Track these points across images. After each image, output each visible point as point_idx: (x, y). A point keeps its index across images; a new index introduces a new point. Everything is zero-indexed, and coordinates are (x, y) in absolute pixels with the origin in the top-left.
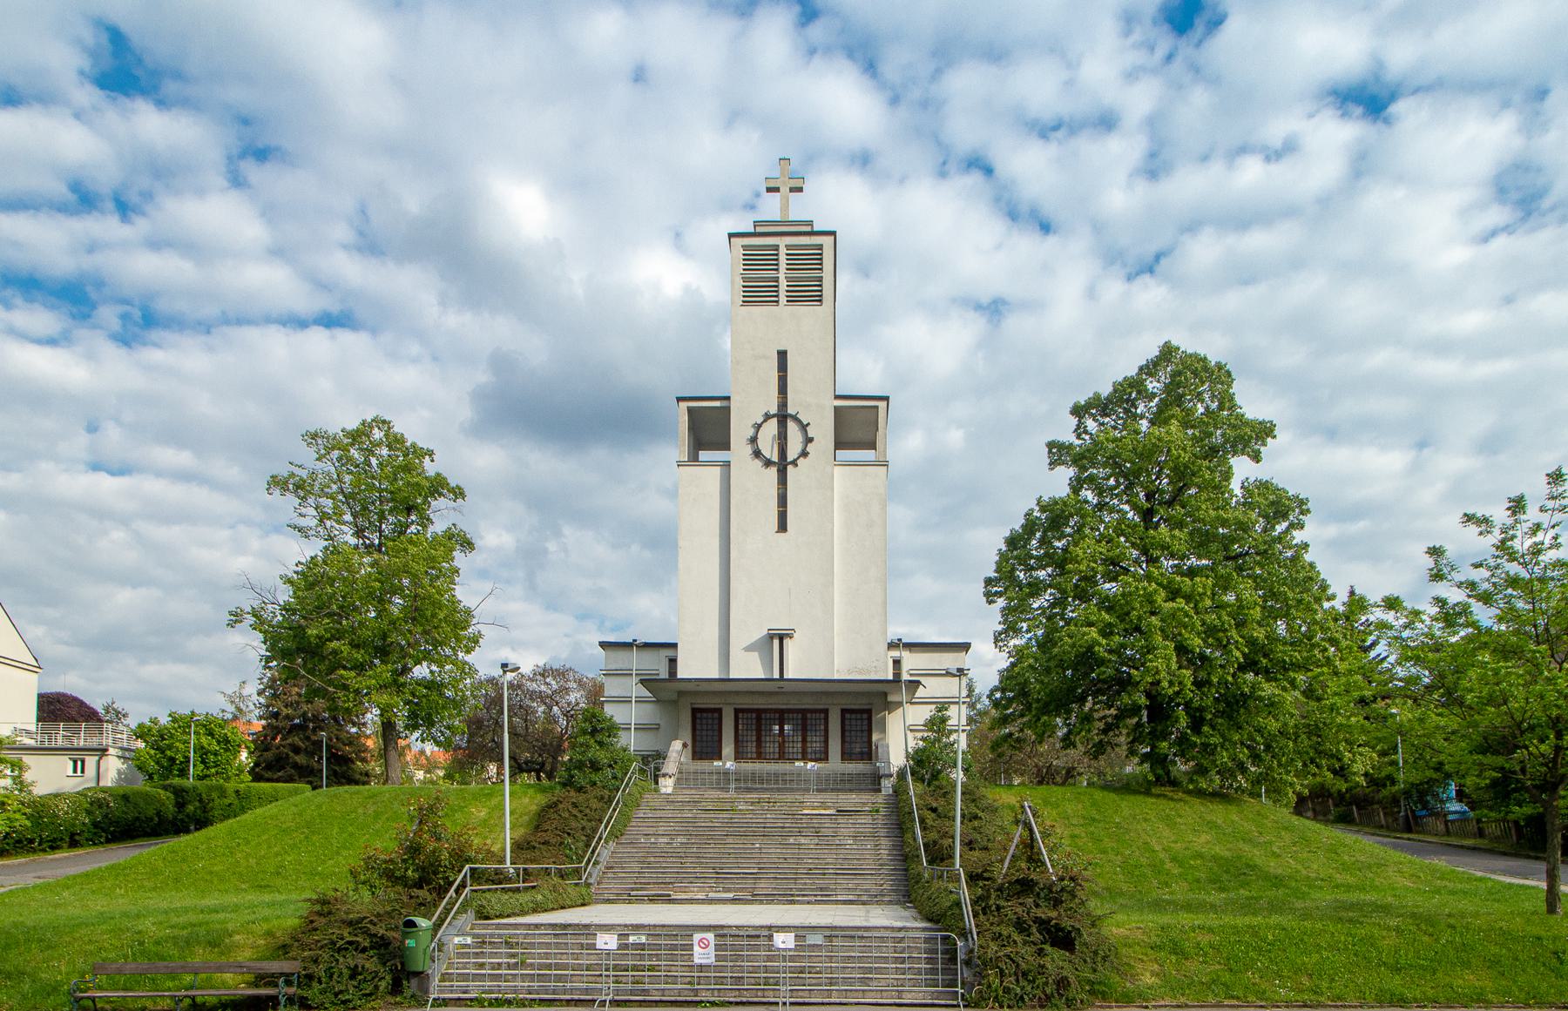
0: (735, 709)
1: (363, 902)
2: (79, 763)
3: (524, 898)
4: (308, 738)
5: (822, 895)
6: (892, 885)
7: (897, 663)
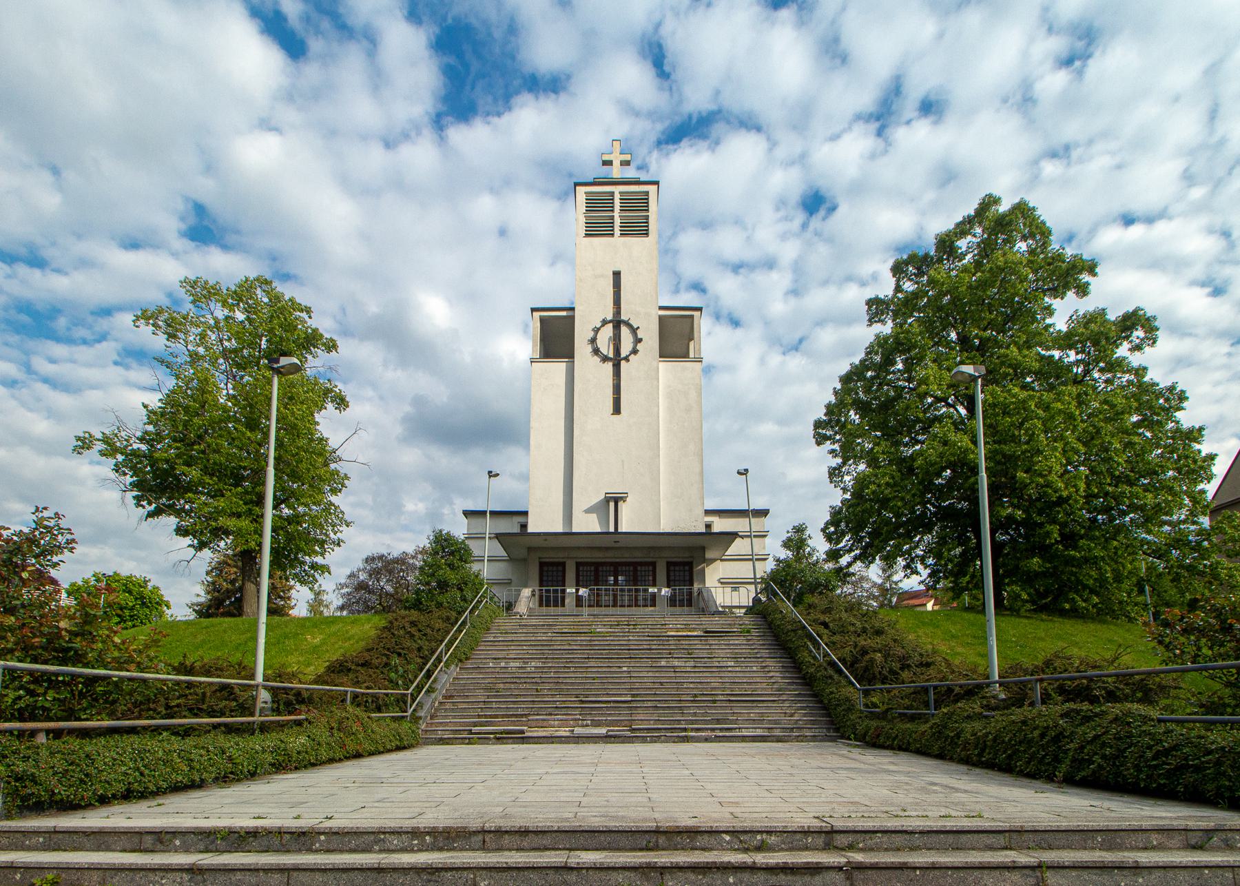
0: (577, 563)
5: (721, 729)
6: (805, 715)
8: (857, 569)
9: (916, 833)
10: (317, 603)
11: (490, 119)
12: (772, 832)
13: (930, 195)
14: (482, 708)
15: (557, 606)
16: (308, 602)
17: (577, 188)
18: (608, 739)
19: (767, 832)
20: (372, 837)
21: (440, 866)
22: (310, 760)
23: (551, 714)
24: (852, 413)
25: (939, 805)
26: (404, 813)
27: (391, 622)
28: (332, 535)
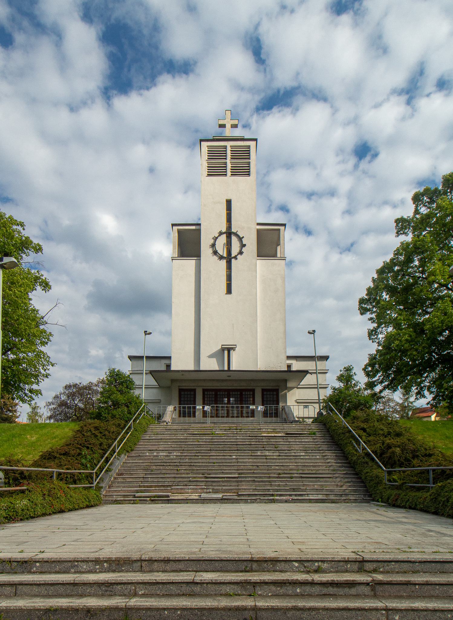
5: (296, 495)
6: (350, 486)
8: (386, 394)
9: (417, 562)
10: (34, 414)
11: (142, 91)
12: (325, 561)
13: (442, 146)
14: (142, 481)
15: (190, 417)
16: (28, 414)
17: (202, 143)
18: (223, 501)
19: (322, 561)
20: (70, 564)
21: (113, 582)
22: (30, 515)
23: (186, 485)
24: (384, 294)
25: (433, 545)
26: (90, 548)
27: (82, 427)
28: (42, 371)
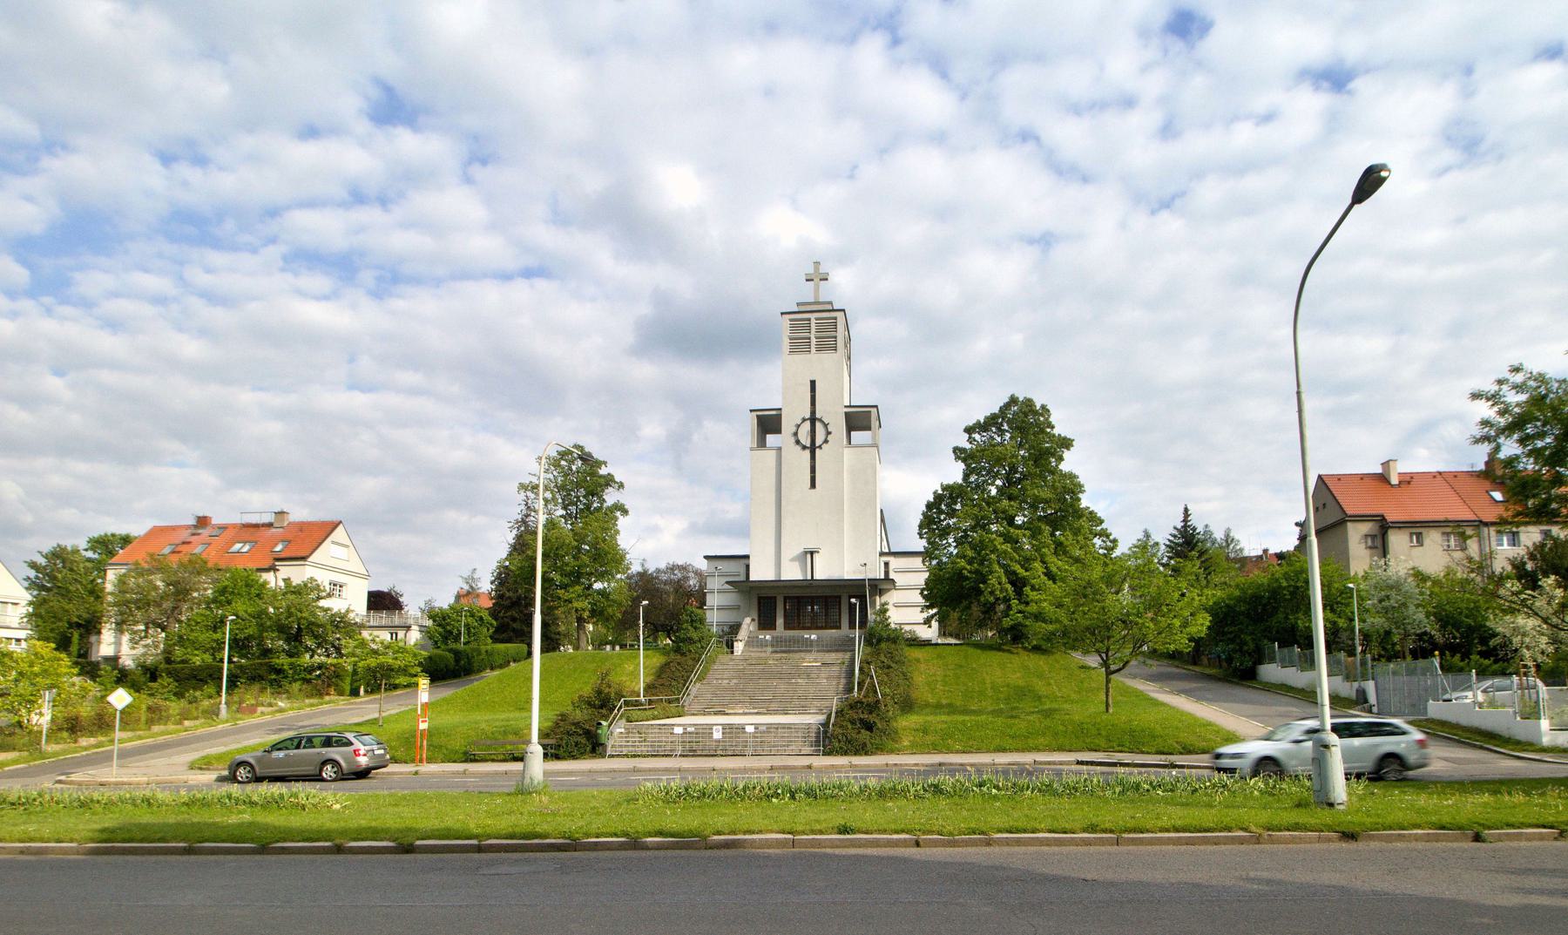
1: (579, 715)
2: (394, 635)
3: (649, 713)
4: (521, 612)
7: (887, 564)
